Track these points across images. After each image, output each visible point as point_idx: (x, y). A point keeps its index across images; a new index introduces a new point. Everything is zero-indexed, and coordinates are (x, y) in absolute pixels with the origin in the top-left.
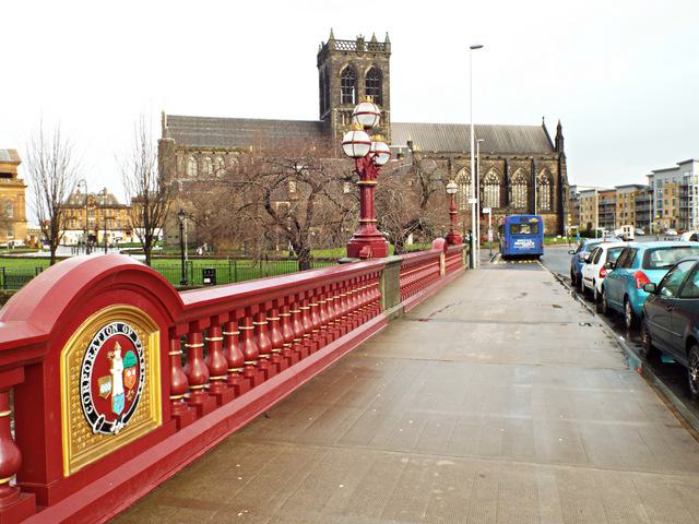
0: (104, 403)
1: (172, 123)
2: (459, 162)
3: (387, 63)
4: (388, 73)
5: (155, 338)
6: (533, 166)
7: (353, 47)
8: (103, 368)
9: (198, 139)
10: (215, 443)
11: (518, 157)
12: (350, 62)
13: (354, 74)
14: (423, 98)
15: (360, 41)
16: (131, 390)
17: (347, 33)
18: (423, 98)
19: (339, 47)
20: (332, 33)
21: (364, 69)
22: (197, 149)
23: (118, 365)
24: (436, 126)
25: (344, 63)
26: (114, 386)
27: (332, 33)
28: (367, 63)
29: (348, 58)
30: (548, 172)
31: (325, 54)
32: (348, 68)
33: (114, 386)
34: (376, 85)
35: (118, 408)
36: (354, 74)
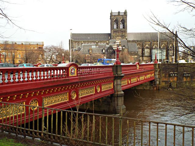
0: (72, 73)
1: (73, 35)
2: (146, 43)
3: (126, 18)
4: (126, 20)
5: (76, 69)
6: (168, 43)
7: (117, 14)
8: (72, 70)
9: (79, 39)
10: (90, 65)
11: (163, 41)
12: (116, 18)
13: (119, 21)
14: (136, 26)
15: (119, 13)
16: (74, 72)
17: (115, 11)
18: (136, 26)
19: (113, 14)
20: (112, 11)
21: (120, 20)
22: (78, 41)
23: (73, 70)
24: (141, 33)
25: (115, 18)
26: (73, 71)
27: (112, 11)
28: (121, 18)
29: (116, 17)
30: (173, 45)
31: (111, 14)
32: (116, 20)
33: (73, 71)
34: (124, 22)
35: (73, 73)
36: (119, 21)
